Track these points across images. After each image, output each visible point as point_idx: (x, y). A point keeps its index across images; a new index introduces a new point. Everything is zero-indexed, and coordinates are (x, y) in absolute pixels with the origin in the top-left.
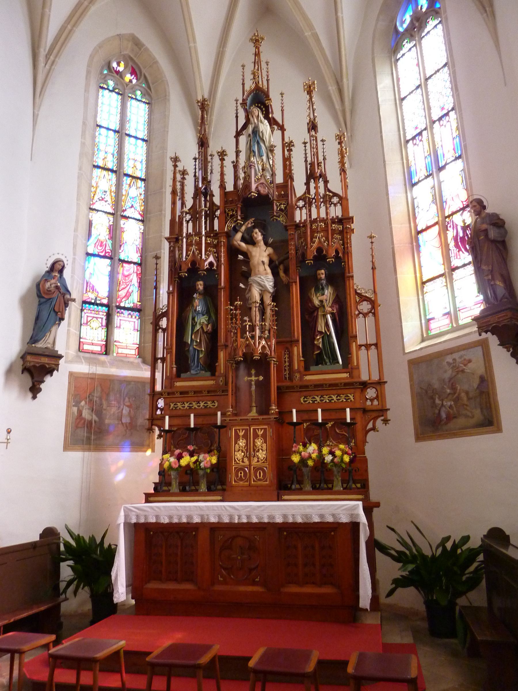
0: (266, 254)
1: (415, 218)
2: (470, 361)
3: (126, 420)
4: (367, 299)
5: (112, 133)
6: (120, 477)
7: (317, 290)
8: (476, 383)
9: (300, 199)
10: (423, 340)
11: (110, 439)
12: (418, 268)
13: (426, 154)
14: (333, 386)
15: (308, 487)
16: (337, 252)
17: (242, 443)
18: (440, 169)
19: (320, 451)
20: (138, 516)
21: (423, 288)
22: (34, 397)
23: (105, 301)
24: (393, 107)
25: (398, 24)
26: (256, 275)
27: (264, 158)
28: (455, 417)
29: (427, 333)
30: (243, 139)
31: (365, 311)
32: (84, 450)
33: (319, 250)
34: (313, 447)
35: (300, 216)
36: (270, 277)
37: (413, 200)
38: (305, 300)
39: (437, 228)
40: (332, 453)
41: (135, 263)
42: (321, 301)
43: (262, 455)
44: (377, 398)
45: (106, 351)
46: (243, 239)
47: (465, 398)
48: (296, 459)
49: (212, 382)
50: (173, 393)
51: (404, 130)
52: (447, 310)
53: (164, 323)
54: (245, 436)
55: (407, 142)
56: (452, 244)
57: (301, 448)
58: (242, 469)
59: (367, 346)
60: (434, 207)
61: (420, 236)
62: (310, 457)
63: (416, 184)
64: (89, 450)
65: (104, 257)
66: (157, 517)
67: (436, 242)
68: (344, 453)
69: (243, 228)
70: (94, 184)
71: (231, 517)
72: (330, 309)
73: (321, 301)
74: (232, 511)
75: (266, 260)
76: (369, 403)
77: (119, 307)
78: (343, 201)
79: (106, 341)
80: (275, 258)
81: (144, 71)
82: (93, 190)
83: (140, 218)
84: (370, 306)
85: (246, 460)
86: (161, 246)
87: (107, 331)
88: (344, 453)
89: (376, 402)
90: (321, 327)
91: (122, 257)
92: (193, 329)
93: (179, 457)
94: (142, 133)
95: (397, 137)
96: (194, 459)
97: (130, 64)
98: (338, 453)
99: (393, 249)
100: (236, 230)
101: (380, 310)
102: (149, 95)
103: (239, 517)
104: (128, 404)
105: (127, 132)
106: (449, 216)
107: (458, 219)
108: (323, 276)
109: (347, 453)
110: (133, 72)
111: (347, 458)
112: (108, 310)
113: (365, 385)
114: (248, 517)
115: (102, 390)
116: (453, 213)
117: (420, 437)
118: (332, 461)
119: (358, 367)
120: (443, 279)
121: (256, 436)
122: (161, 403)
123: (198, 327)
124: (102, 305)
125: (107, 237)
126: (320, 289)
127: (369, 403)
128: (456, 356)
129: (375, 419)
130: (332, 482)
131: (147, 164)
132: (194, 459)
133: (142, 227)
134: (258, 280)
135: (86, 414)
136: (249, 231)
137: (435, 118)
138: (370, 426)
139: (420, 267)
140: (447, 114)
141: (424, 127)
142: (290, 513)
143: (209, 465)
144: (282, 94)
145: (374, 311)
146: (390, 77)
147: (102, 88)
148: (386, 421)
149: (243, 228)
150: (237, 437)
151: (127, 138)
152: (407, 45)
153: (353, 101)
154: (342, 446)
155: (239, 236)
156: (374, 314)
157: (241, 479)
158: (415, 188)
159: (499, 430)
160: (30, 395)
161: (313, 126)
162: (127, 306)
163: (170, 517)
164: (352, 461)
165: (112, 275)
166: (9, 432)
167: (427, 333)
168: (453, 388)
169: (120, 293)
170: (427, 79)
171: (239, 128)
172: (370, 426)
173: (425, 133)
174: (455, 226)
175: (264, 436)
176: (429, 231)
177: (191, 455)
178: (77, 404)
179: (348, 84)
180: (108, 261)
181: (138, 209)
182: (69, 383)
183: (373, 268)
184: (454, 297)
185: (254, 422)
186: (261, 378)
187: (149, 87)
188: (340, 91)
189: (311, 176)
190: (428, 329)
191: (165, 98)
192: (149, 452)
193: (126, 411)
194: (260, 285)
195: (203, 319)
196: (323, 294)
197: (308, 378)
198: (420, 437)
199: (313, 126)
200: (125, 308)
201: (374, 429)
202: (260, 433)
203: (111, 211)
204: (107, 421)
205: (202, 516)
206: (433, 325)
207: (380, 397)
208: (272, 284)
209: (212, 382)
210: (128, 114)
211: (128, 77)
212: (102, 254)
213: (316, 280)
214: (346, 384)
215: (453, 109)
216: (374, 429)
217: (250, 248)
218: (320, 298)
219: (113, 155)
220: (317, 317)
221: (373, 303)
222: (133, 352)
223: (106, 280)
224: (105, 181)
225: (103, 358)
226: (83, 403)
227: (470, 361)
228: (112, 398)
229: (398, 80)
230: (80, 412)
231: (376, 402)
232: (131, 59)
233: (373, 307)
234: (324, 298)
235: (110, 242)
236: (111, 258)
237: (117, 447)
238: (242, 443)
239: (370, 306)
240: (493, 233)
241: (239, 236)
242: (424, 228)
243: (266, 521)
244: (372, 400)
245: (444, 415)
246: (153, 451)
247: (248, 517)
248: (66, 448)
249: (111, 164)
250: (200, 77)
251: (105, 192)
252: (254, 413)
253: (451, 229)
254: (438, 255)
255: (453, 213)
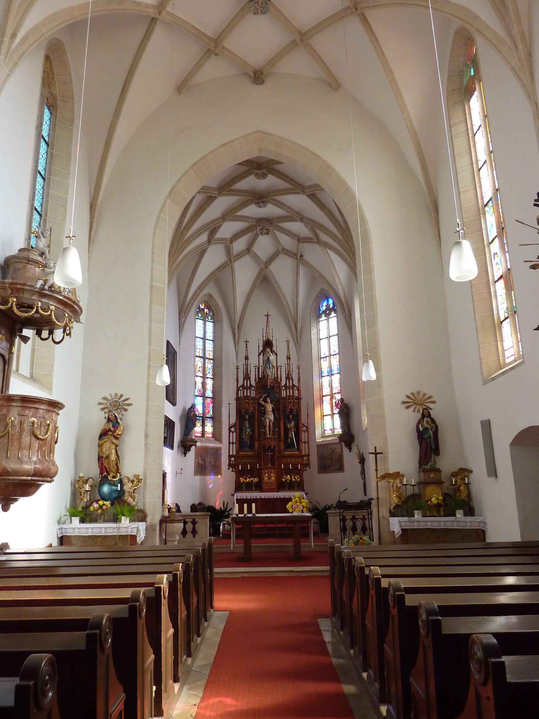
0: (271, 407)
1: (322, 390)
2: (337, 448)
3: (212, 464)
4: (305, 426)
5: (201, 339)
6: (211, 486)
7: (289, 422)
8: (338, 456)
9: (283, 386)
10: (322, 437)
11: (208, 471)
12: (322, 410)
13: (328, 367)
14: (294, 456)
15: (287, 489)
16: (296, 410)
17: (267, 475)
18: (332, 375)
19: (291, 478)
20: (240, 497)
21: (323, 417)
22: (185, 456)
23: (202, 415)
24: (317, 342)
25: (320, 307)
26: (268, 415)
27: (271, 370)
28: (331, 466)
29: (324, 435)
30: (261, 356)
31: (304, 430)
32: (200, 476)
33: (291, 409)
34: (289, 476)
35: (284, 394)
36: (273, 416)
37: (322, 382)
38: (285, 426)
39: (329, 396)
40: (295, 478)
41: (211, 398)
42: (290, 427)
43: (273, 478)
44: (307, 460)
45: (203, 436)
46: (262, 401)
47: (334, 461)
48: (284, 480)
49: (253, 453)
50: (239, 457)
51: (320, 353)
52: (331, 428)
53: (233, 429)
54: (268, 473)
55: (321, 358)
56: (334, 405)
57: (285, 477)
58: (266, 483)
59: (305, 442)
60: (329, 388)
61: (323, 397)
62: (288, 479)
63: (323, 377)
64: (202, 475)
65: (201, 396)
66: (265, 496)
67: (329, 402)
68: (298, 478)
69: (263, 397)
70: (196, 365)
71: (268, 496)
72: (293, 430)
73: (290, 427)
74: (269, 495)
75: (271, 410)
76: (304, 462)
77: (207, 417)
78: (298, 389)
79: (202, 432)
80: (274, 408)
81: (212, 307)
82: (196, 367)
83: (212, 377)
84: (306, 429)
85: (268, 480)
86: (221, 391)
87: (203, 428)
88: (298, 478)
89: (307, 462)
90: (290, 436)
91: (207, 395)
92: (245, 434)
93: (246, 479)
94: (211, 338)
95: (317, 355)
96: (251, 479)
97: (207, 304)
98: (296, 478)
99: (314, 401)
100: (261, 397)
101: (310, 430)
102: (214, 318)
103: (271, 496)
104: (213, 457)
105: (206, 338)
106: (334, 394)
107: (336, 395)
108: (291, 417)
109: (299, 478)
110: (208, 308)
111: (299, 480)
112: (203, 419)
113: (304, 456)
114: (273, 496)
115: (205, 453)
116: (335, 394)
117: (320, 472)
118: (295, 480)
119: (302, 450)
120: (326, 320)
121: (271, 473)
122: (233, 459)
123: (247, 433)
124: (201, 417)
125: (201, 387)
126: (290, 422)
127: (304, 462)
128: (332, 446)
129: (306, 467)
130: (242, 488)
131: (214, 352)
132: (251, 479)
133: (213, 381)
134: (269, 417)
135: (200, 462)
136: (266, 397)
137: (332, 354)
138: (305, 469)
139: (323, 409)
140: (336, 355)
141: (328, 355)
142: (285, 495)
143: (256, 482)
144: (267, 316)
145: (307, 430)
146: (316, 329)
147: (197, 318)
148: (310, 468)
149: (263, 397)
150: (265, 473)
151: (206, 340)
152: (323, 318)
153: (301, 332)
154: (297, 476)
155: (262, 399)
156: (307, 432)
157: (267, 486)
158: (323, 378)
159: (344, 472)
160: (184, 455)
161: (288, 358)
162: (209, 416)
163: (250, 497)
164: (300, 480)
165: (204, 404)
166: (182, 469)
167: (324, 435)
168: (331, 457)
169: (206, 411)
170: (330, 337)
171: (260, 352)
172: (305, 469)
173: (328, 358)
174: (335, 398)
175: (274, 473)
176: (327, 397)
177: (249, 479)
178: (197, 458)
179: (299, 326)
180: (202, 398)
181: (211, 374)
182: (195, 450)
183: (308, 415)
184: (333, 424)
185: (271, 468)
186: (272, 454)
187: (214, 315)
188: (296, 327)
189: (288, 378)
190: (324, 433)
191: (221, 321)
192: (219, 476)
193: (212, 460)
194: (269, 419)
195: (249, 430)
196: (291, 424)
197: (286, 453)
198: (320, 472)
199: (288, 358)
200: (208, 418)
201: (306, 470)
202: (273, 472)
203: (202, 376)
204: (207, 464)
205: (260, 496)
206: (326, 432)
207: (308, 460)
208: (273, 418)
209: (253, 453)
210: (207, 329)
211: (206, 310)
212: (200, 395)
213: (289, 418)
214: (298, 456)
215: (338, 354)
216: (306, 470)
217: (265, 404)
218: (290, 425)
219: (202, 350)
220: (289, 432)
221: (307, 427)
222: (211, 436)
223: (201, 406)
224: (199, 362)
225: (202, 439)
226: (199, 457)
227: (337, 448)
228: (208, 455)
229: (319, 330)
230: (198, 461)
231: (307, 462)
232: (207, 302)
233: (307, 429)
234: (292, 425)
235: (202, 390)
236: (203, 397)
237: (209, 474)
238: (267, 475)
239: (306, 429)
240: (345, 411)
241: (262, 399)
242: (325, 395)
243: (278, 497)
244: (305, 461)
245: (328, 466)
246: (221, 476)
247: (273, 496)
248: (195, 475)
249: (201, 355)
250: (237, 313)
251: (200, 367)
252: (270, 465)
253: (334, 399)
254: (329, 407)
255: (335, 394)
